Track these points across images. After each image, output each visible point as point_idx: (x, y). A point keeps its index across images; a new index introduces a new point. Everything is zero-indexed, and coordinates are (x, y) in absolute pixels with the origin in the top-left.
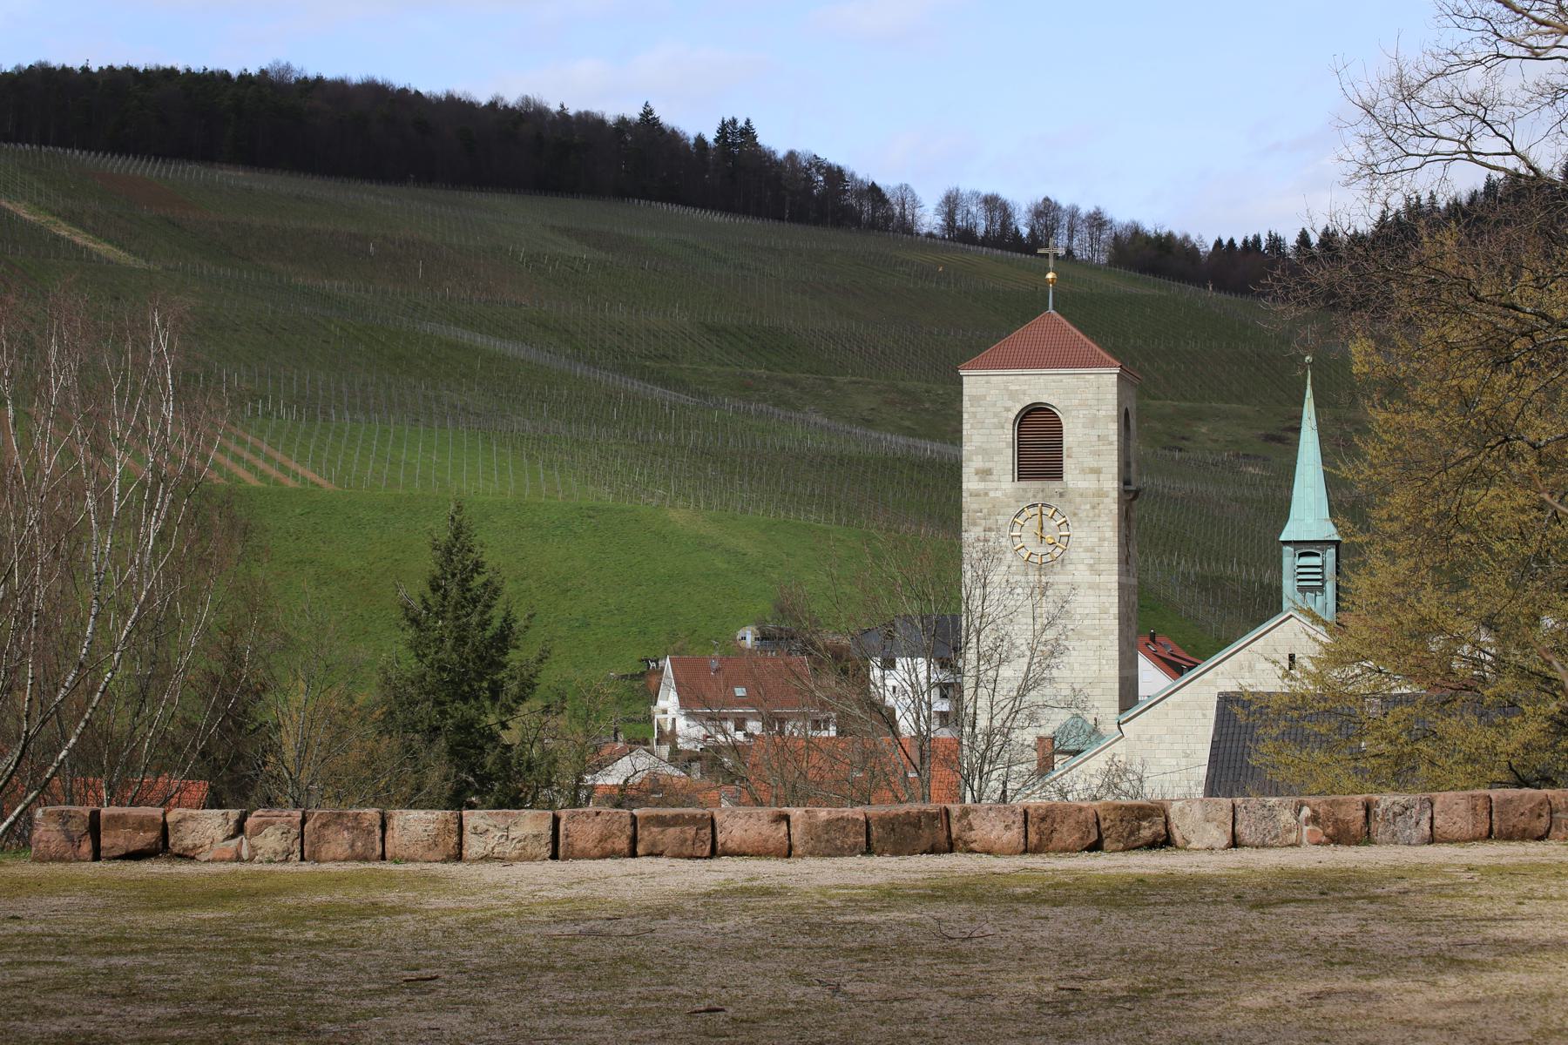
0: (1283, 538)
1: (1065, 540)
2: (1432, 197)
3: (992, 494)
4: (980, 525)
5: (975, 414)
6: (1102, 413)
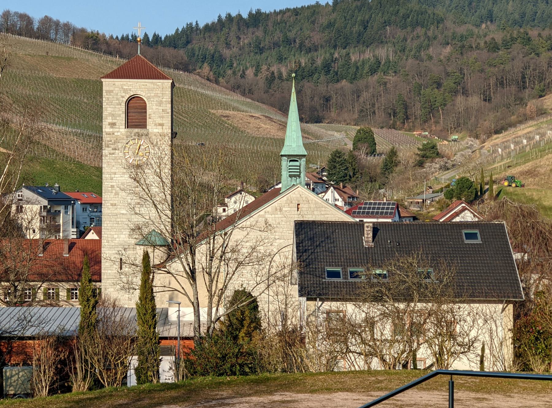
1: (148, 154)
2: (197, 24)
3: (116, 134)
4: (111, 147)
5: (108, 99)
6: (164, 100)
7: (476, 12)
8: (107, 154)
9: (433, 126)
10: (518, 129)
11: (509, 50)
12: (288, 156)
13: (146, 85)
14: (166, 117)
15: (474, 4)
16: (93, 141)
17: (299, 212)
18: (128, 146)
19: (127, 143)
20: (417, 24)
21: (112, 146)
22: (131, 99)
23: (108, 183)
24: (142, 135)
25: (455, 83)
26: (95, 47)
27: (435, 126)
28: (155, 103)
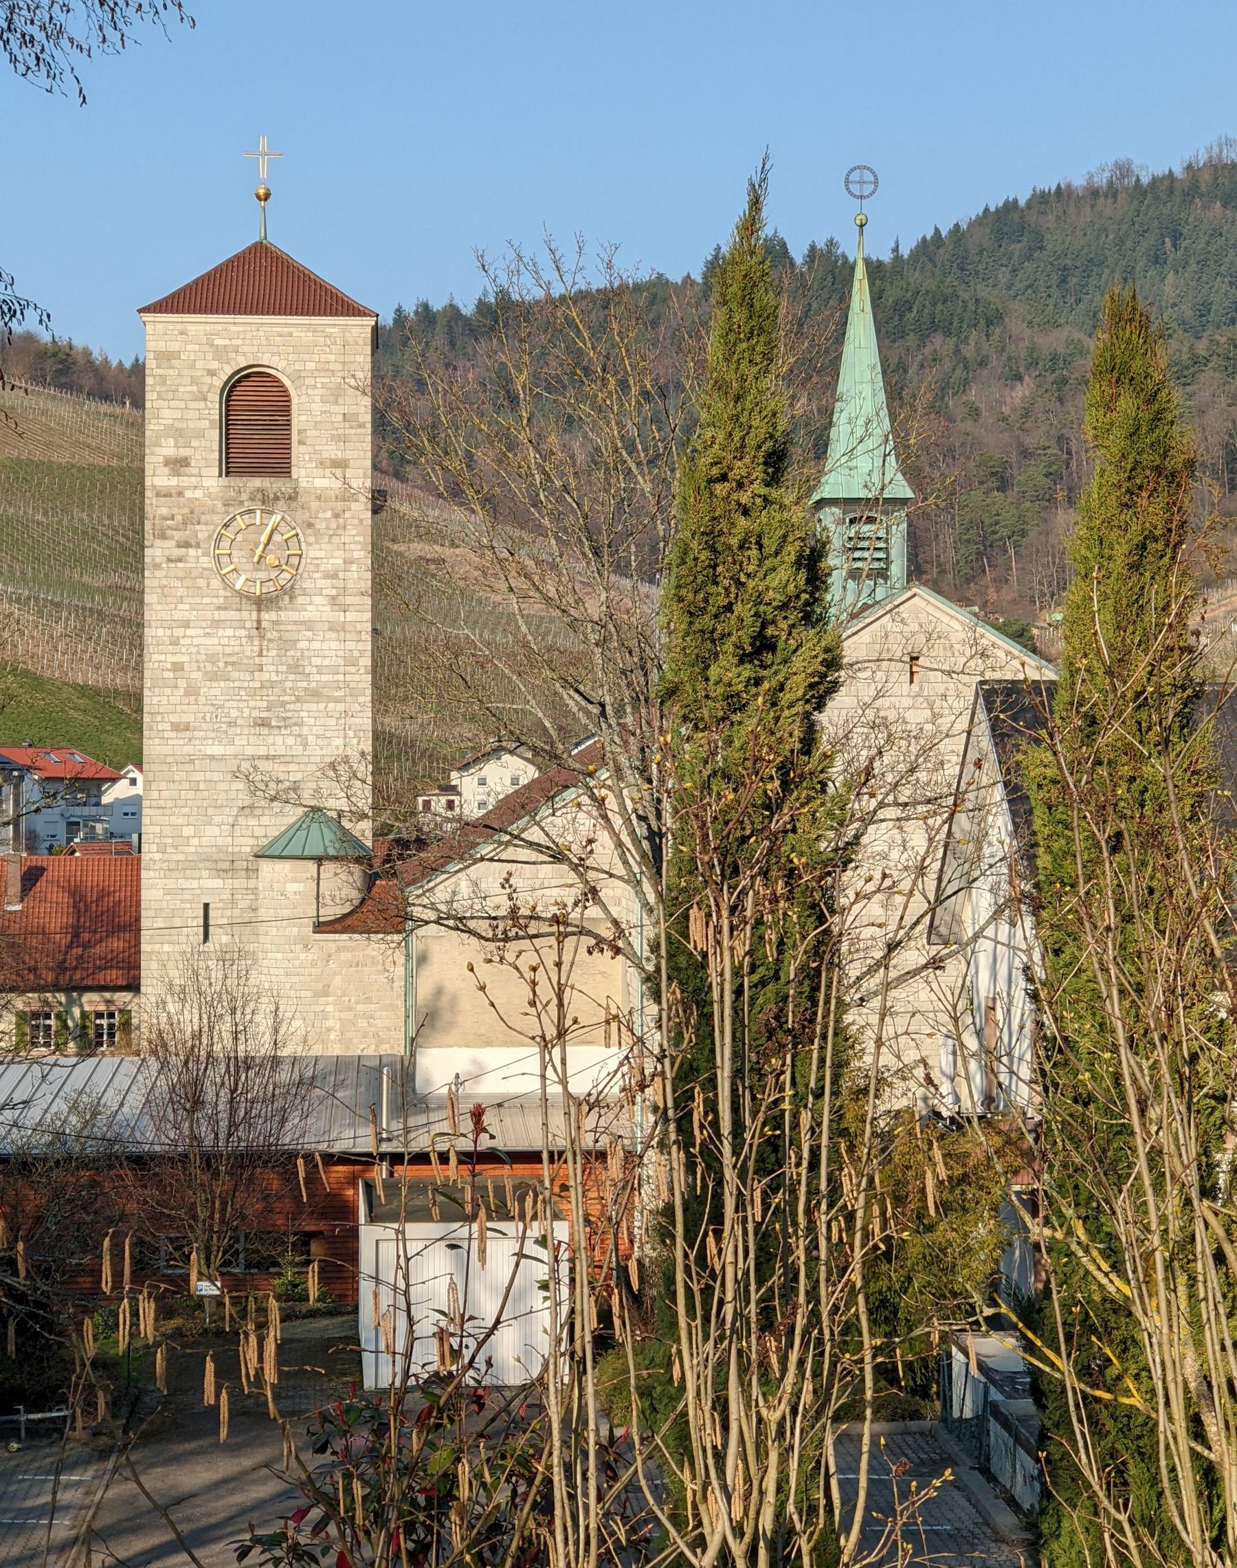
0: (826, 492)
1: (295, 561)
3: (189, 494)
4: (172, 538)
7: (1078, 301)
8: (158, 560)
9: (991, 590)
10: (1229, 592)
11: (1189, 389)
12: (848, 503)
13: (291, 335)
14: (354, 438)
15: (1074, 280)
16: (67, 619)
17: (915, 687)
18: (229, 533)
19: (226, 526)
20: (934, 326)
21: (178, 535)
22: (239, 381)
23: (163, 657)
24: (277, 498)
25: (1049, 474)
26: (64, 380)
27: (998, 591)
28: (320, 392)
